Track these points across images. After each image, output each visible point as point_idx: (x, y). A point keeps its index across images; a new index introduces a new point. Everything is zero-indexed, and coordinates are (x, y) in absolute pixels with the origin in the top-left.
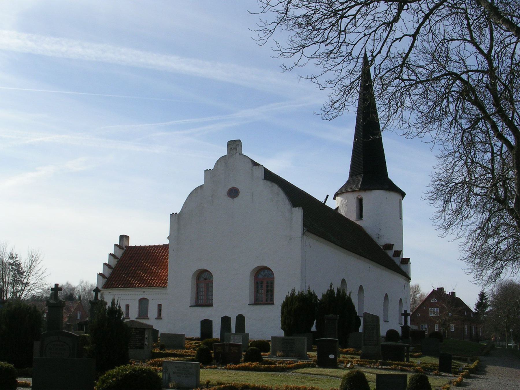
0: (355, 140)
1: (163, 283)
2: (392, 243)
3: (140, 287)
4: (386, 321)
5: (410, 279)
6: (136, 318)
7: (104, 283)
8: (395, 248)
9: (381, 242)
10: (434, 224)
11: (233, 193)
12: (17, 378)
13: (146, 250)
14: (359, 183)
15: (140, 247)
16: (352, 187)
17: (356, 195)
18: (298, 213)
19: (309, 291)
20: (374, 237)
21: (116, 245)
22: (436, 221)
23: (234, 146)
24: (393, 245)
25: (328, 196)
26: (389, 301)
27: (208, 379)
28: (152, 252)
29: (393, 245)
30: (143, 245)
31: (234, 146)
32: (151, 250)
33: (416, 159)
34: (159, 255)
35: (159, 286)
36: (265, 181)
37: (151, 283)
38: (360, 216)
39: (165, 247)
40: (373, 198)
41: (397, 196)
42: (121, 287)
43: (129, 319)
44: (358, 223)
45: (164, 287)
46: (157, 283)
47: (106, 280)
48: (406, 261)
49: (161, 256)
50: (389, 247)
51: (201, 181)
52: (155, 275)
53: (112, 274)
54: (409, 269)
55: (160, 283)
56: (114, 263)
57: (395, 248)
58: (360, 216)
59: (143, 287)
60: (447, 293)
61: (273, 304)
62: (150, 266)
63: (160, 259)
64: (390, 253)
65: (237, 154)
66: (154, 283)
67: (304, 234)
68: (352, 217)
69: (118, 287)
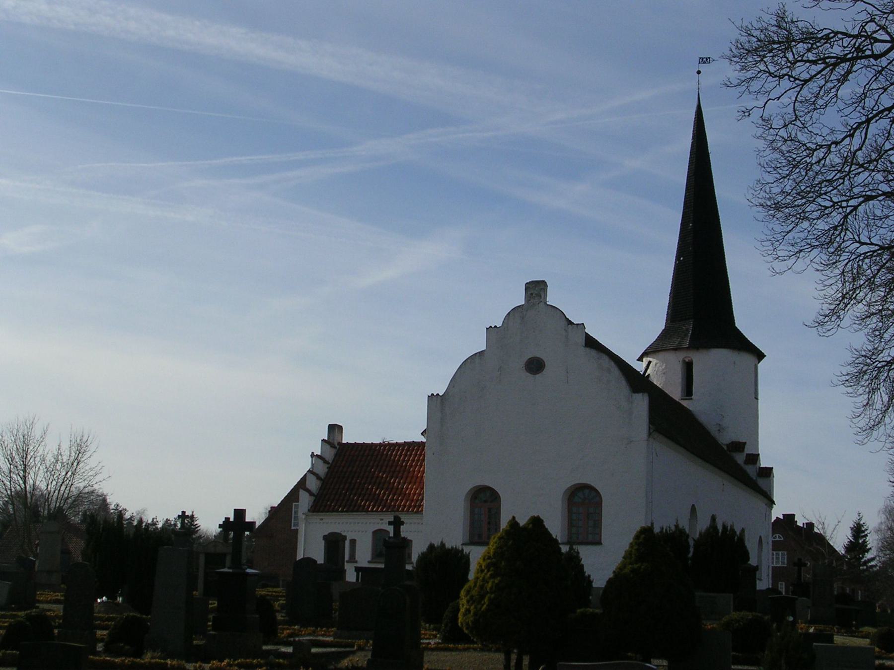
0: (678, 258)
1: (415, 506)
3: (376, 511)
6: (369, 562)
7: (311, 503)
8: (748, 450)
9: (725, 439)
10: (853, 426)
11: (535, 366)
13: (375, 450)
14: (686, 335)
15: (364, 445)
16: (676, 342)
17: (681, 356)
18: (642, 402)
19: (677, 526)
20: (713, 429)
21: (323, 440)
22: (855, 421)
23: (536, 290)
27: (487, 655)
28: (387, 454)
30: (368, 441)
31: (536, 290)
32: (384, 450)
33: (771, 287)
34: (399, 460)
35: (408, 511)
36: (588, 349)
37: (395, 506)
38: (688, 391)
39: (413, 449)
40: (711, 363)
41: (748, 358)
42: (342, 511)
43: (356, 562)
44: (685, 403)
45: (417, 512)
46: (405, 506)
47: (313, 498)
48: (767, 473)
49: (404, 460)
50: (739, 446)
51: (481, 345)
52: (398, 492)
53: (321, 488)
55: (410, 506)
56: (322, 469)
57: (748, 450)
58: (688, 391)
59: (382, 511)
60: (800, 524)
61: (599, 543)
62: (387, 477)
63: (402, 466)
64: (740, 458)
65: (542, 304)
66: (399, 506)
67: (650, 434)
68: (675, 392)
69: (337, 511)
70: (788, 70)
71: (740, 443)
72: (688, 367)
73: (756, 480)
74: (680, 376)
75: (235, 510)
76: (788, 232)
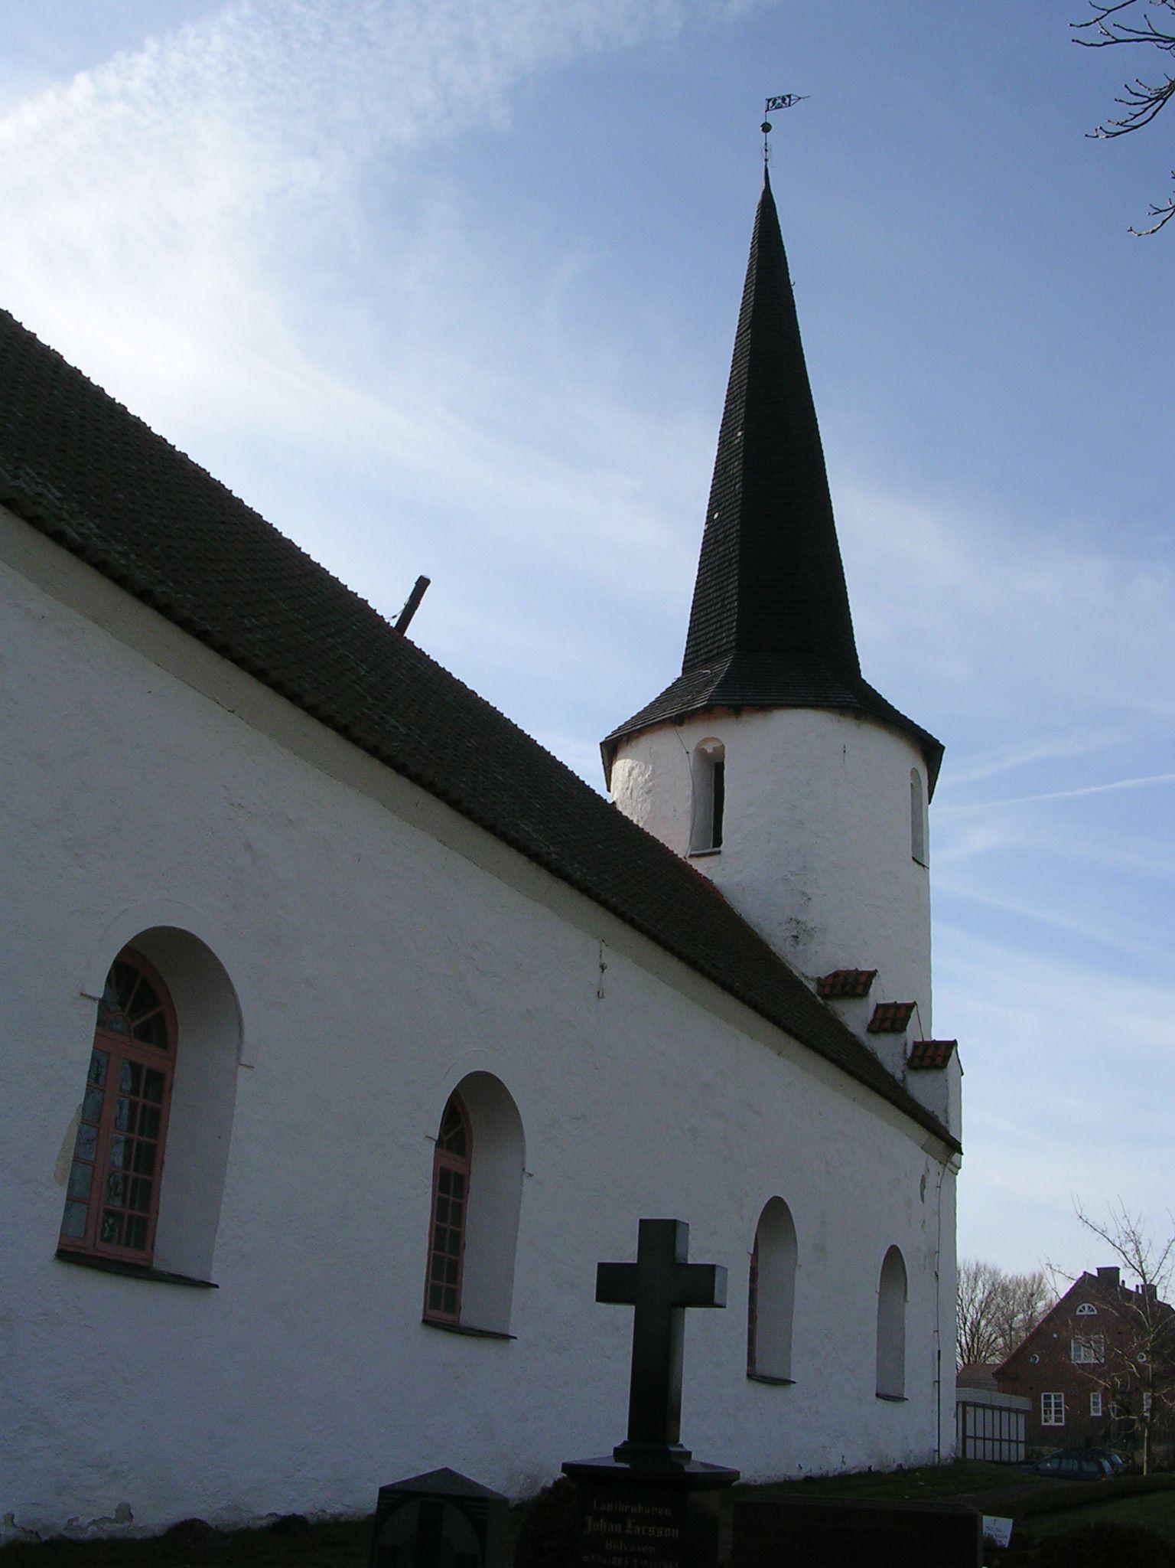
0: (709, 518)
2: (865, 967)
4: (765, 1376)
5: (955, 1147)
8: (882, 992)
9: (812, 964)
12: (1002, 1547)
24: (872, 974)
25: (422, 584)
26: (804, 1249)
29: (872, 974)
40: (780, 749)
44: (701, 866)
48: (938, 1056)
50: (853, 984)
54: (951, 1096)
57: (882, 992)
58: (713, 836)
64: (855, 1017)
68: (676, 834)
70: (1056, 1461)
71: (857, 973)
72: (713, 770)
73: (903, 1078)
74: (689, 792)
75: (643, 1223)
76: (1118, 41)
